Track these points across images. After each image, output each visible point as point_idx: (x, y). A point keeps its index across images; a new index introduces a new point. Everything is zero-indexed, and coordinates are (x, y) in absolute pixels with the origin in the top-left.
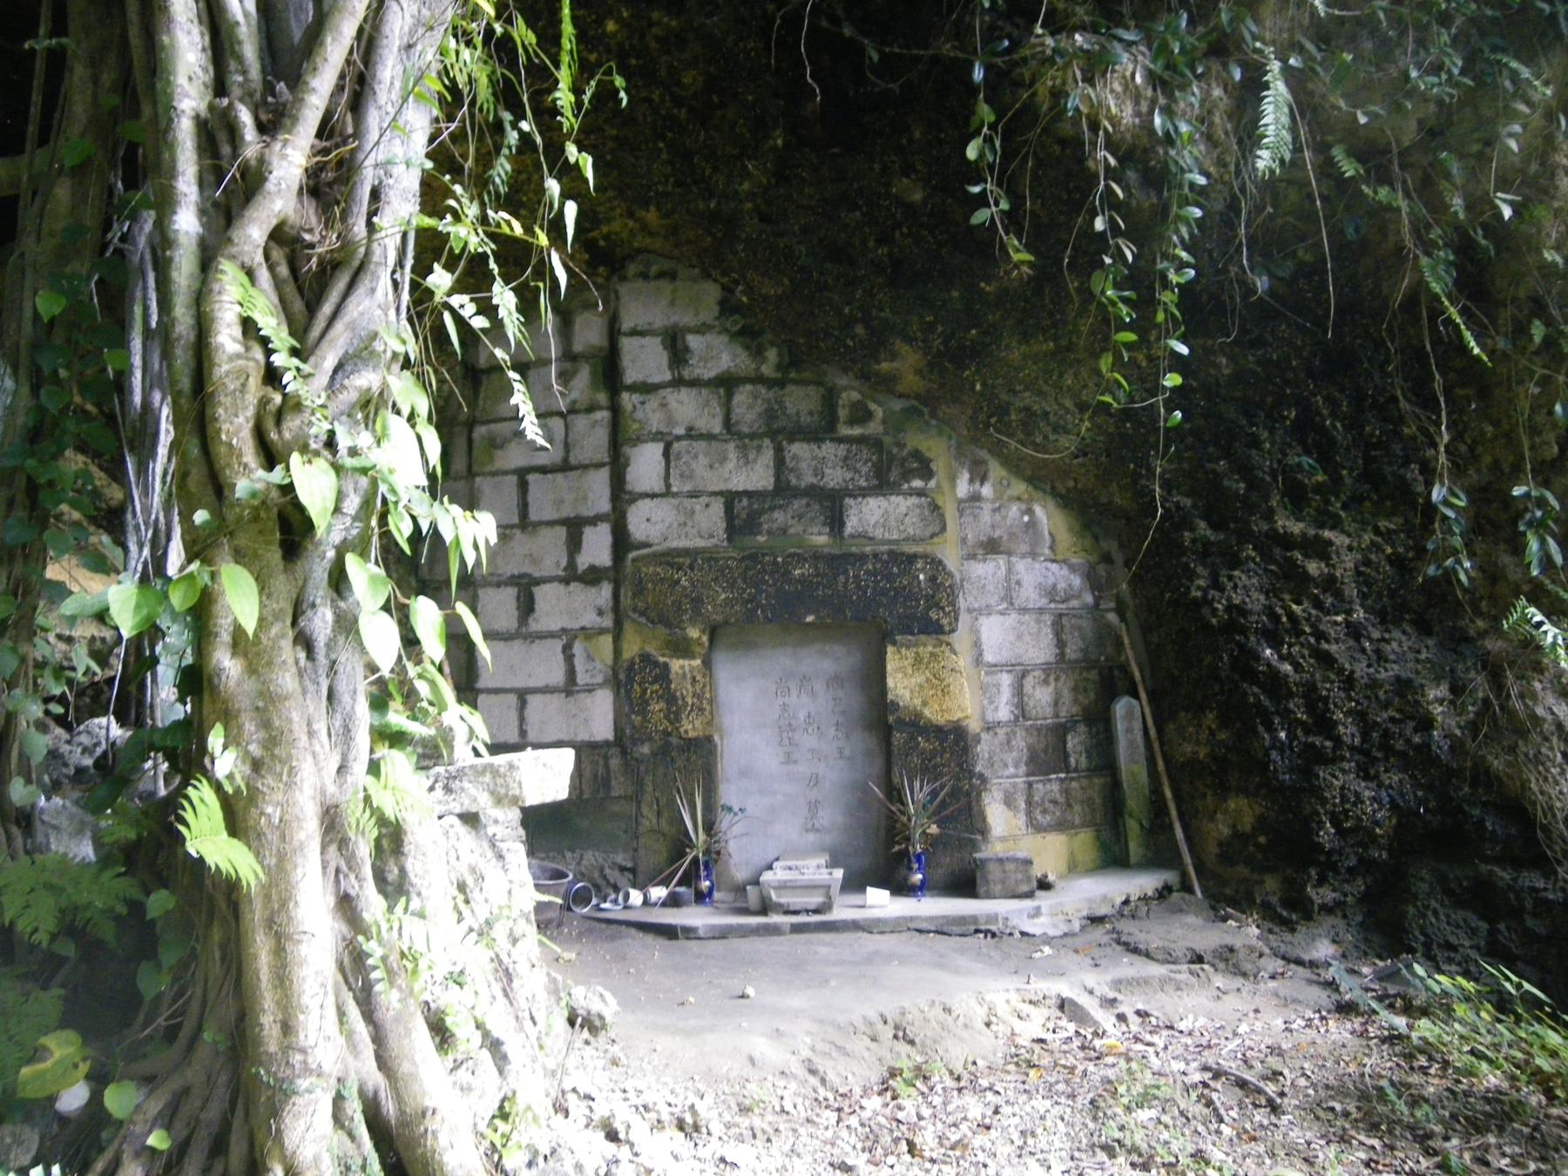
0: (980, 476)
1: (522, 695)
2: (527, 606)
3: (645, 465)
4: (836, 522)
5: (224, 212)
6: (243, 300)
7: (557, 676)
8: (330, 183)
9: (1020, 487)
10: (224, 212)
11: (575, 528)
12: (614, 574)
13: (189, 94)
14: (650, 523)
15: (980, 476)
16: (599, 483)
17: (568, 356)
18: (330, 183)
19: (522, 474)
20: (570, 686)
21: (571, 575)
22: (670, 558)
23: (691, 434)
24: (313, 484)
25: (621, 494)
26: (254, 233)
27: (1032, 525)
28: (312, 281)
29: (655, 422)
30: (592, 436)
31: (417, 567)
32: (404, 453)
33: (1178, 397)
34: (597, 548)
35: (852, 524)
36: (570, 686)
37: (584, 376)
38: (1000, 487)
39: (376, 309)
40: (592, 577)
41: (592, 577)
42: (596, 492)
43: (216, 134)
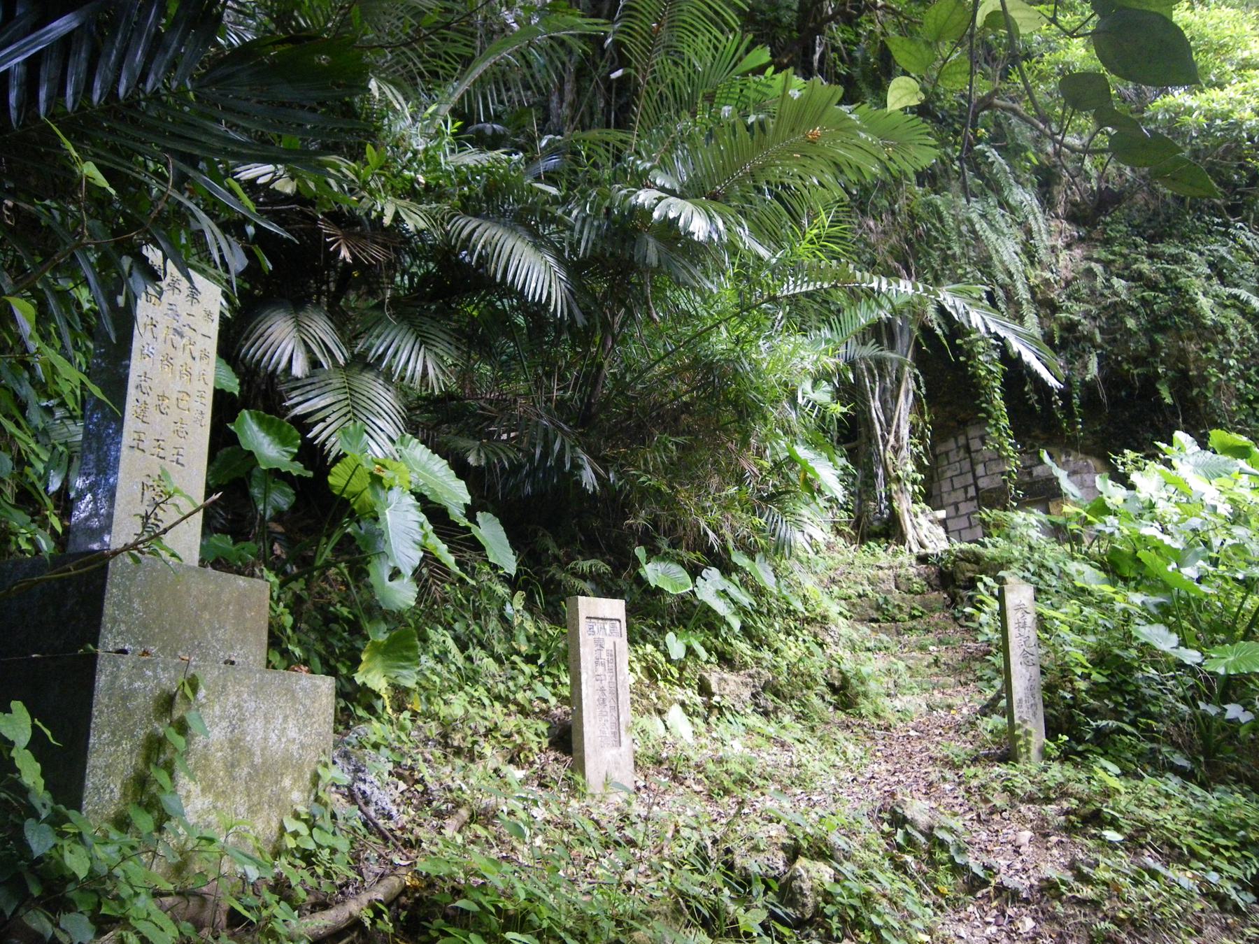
0: (1068, 455)
1: (959, 531)
2: (957, 509)
3: (980, 469)
4: (1030, 474)
5: (885, 446)
6: (889, 454)
7: (967, 525)
8: (897, 439)
9: (1080, 456)
10: (885, 446)
11: (966, 488)
12: (977, 497)
13: (879, 432)
14: (984, 483)
15: (1068, 455)
16: (970, 476)
17: (958, 447)
18: (897, 439)
19: (951, 478)
20: (971, 526)
21: (967, 500)
22: (990, 491)
23: (990, 460)
24: (900, 473)
25: (975, 478)
26: (889, 447)
27: (1088, 465)
28: (896, 451)
29: (981, 458)
30: (966, 465)
31: (914, 482)
32: (910, 467)
33: (1082, 430)
34: (972, 492)
35: (1035, 474)
36: (971, 526)
37: (962, 452)
38: (1075, 458)
39: (904, 453)
40: (972, 499)
41: (972, 499)
42: (970, 479)
43: (883, 436)
